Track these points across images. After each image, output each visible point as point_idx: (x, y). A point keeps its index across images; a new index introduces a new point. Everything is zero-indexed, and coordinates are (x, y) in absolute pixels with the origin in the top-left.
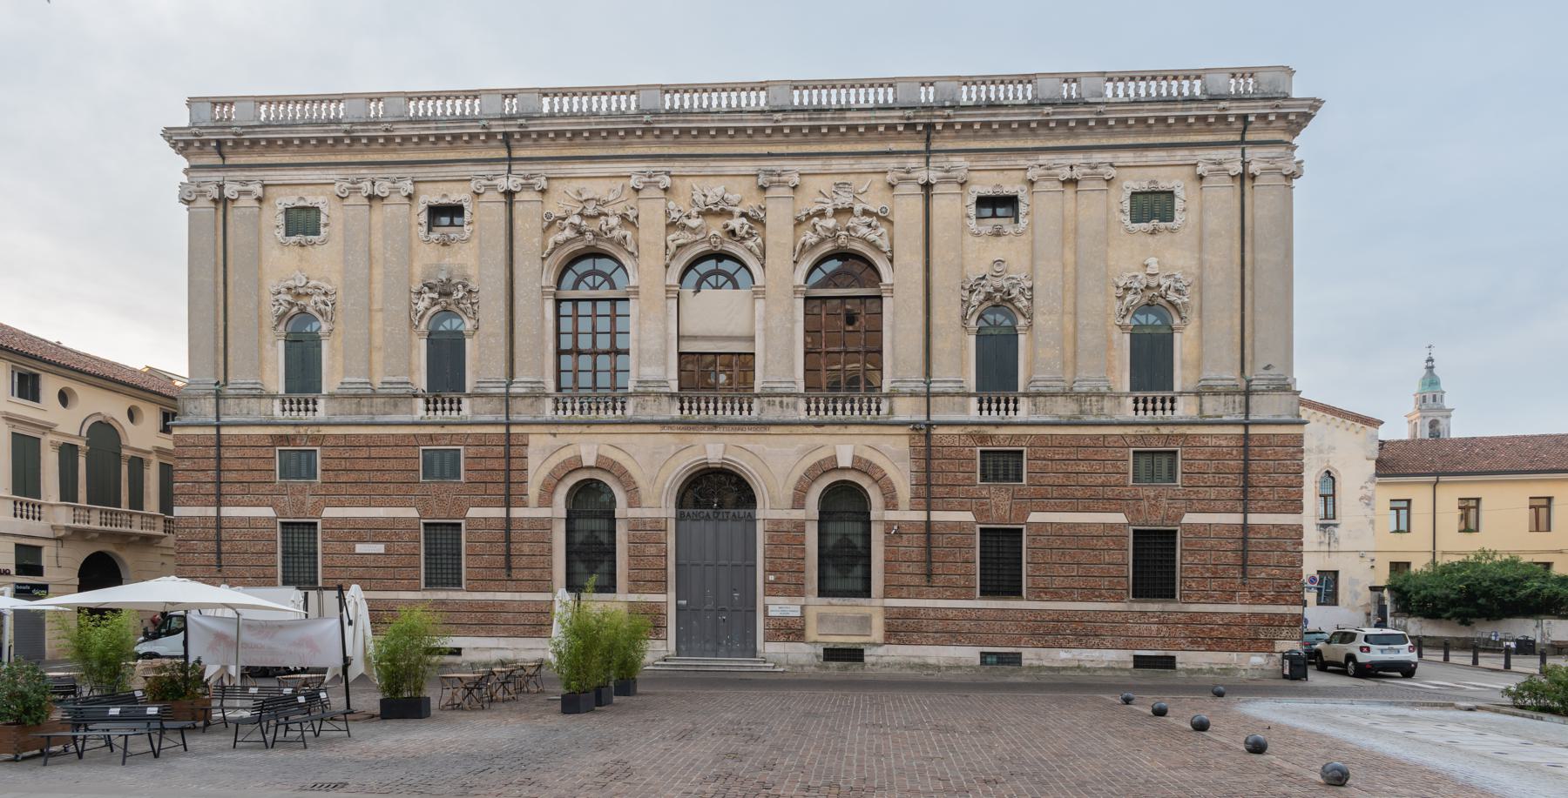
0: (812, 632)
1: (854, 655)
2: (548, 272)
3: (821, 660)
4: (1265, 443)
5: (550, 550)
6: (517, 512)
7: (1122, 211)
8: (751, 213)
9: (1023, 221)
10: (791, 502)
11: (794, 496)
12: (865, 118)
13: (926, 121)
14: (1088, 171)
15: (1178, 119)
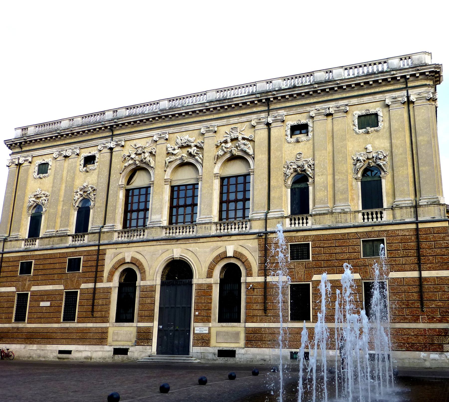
0: (213, 342)
1: (231, 353)
2: (122, 179)
3: (217, 356)
4: (428, 232)
5: (110, 302)
6: (99, 285)
7: (354, 125)
8: (198, 145)
9: (310, 134)
10: (206, 275)
11: (208, 271)
12: (241, 100)
13: (266, 98)
14: (337, 109)
15: (374, 82)
